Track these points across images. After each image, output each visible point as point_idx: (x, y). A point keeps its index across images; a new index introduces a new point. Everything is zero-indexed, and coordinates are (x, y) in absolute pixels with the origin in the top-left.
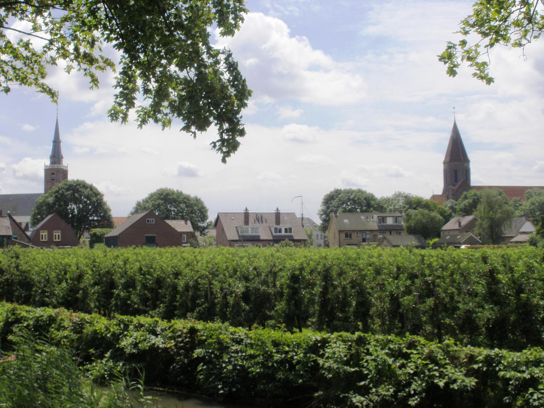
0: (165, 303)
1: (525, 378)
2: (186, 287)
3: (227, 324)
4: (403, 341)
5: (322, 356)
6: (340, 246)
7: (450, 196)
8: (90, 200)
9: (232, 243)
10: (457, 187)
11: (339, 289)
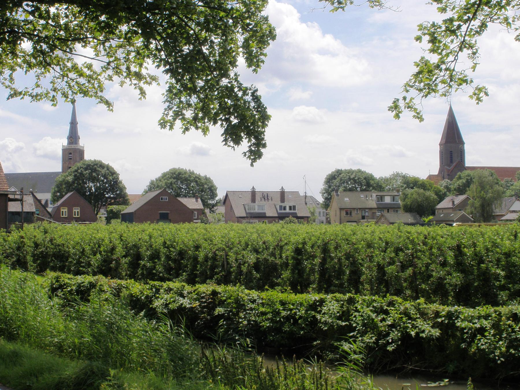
0: (187, 272)
1: (476, 327)
2: (205, 258)
3: (243, 287)
4: (385, 300)
5: (319, 312)
6: (340, 223)
7: (446, 176)
8: (107, 178)
9: (240, 219)
10: (452, 167)
11: (336, 261)
